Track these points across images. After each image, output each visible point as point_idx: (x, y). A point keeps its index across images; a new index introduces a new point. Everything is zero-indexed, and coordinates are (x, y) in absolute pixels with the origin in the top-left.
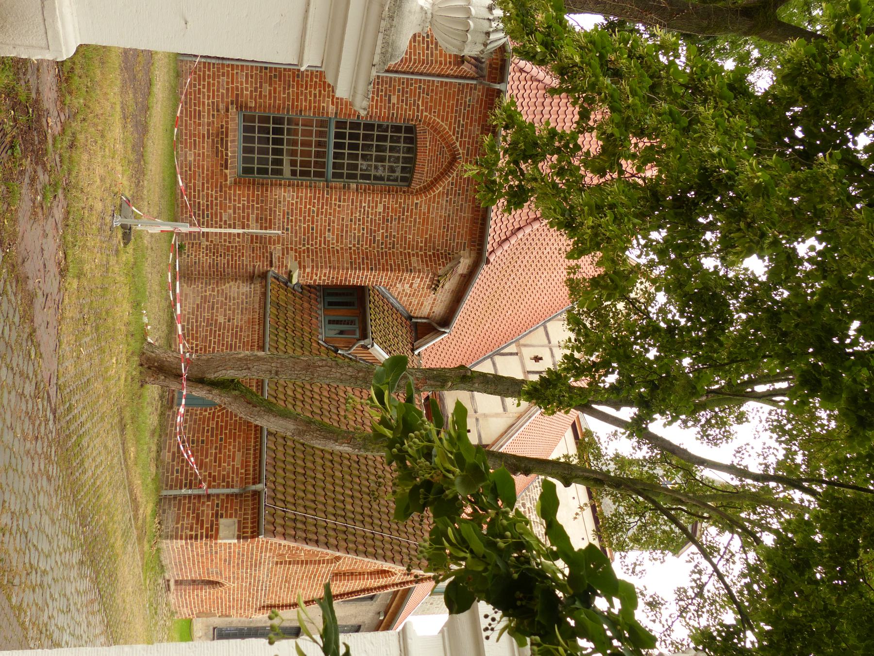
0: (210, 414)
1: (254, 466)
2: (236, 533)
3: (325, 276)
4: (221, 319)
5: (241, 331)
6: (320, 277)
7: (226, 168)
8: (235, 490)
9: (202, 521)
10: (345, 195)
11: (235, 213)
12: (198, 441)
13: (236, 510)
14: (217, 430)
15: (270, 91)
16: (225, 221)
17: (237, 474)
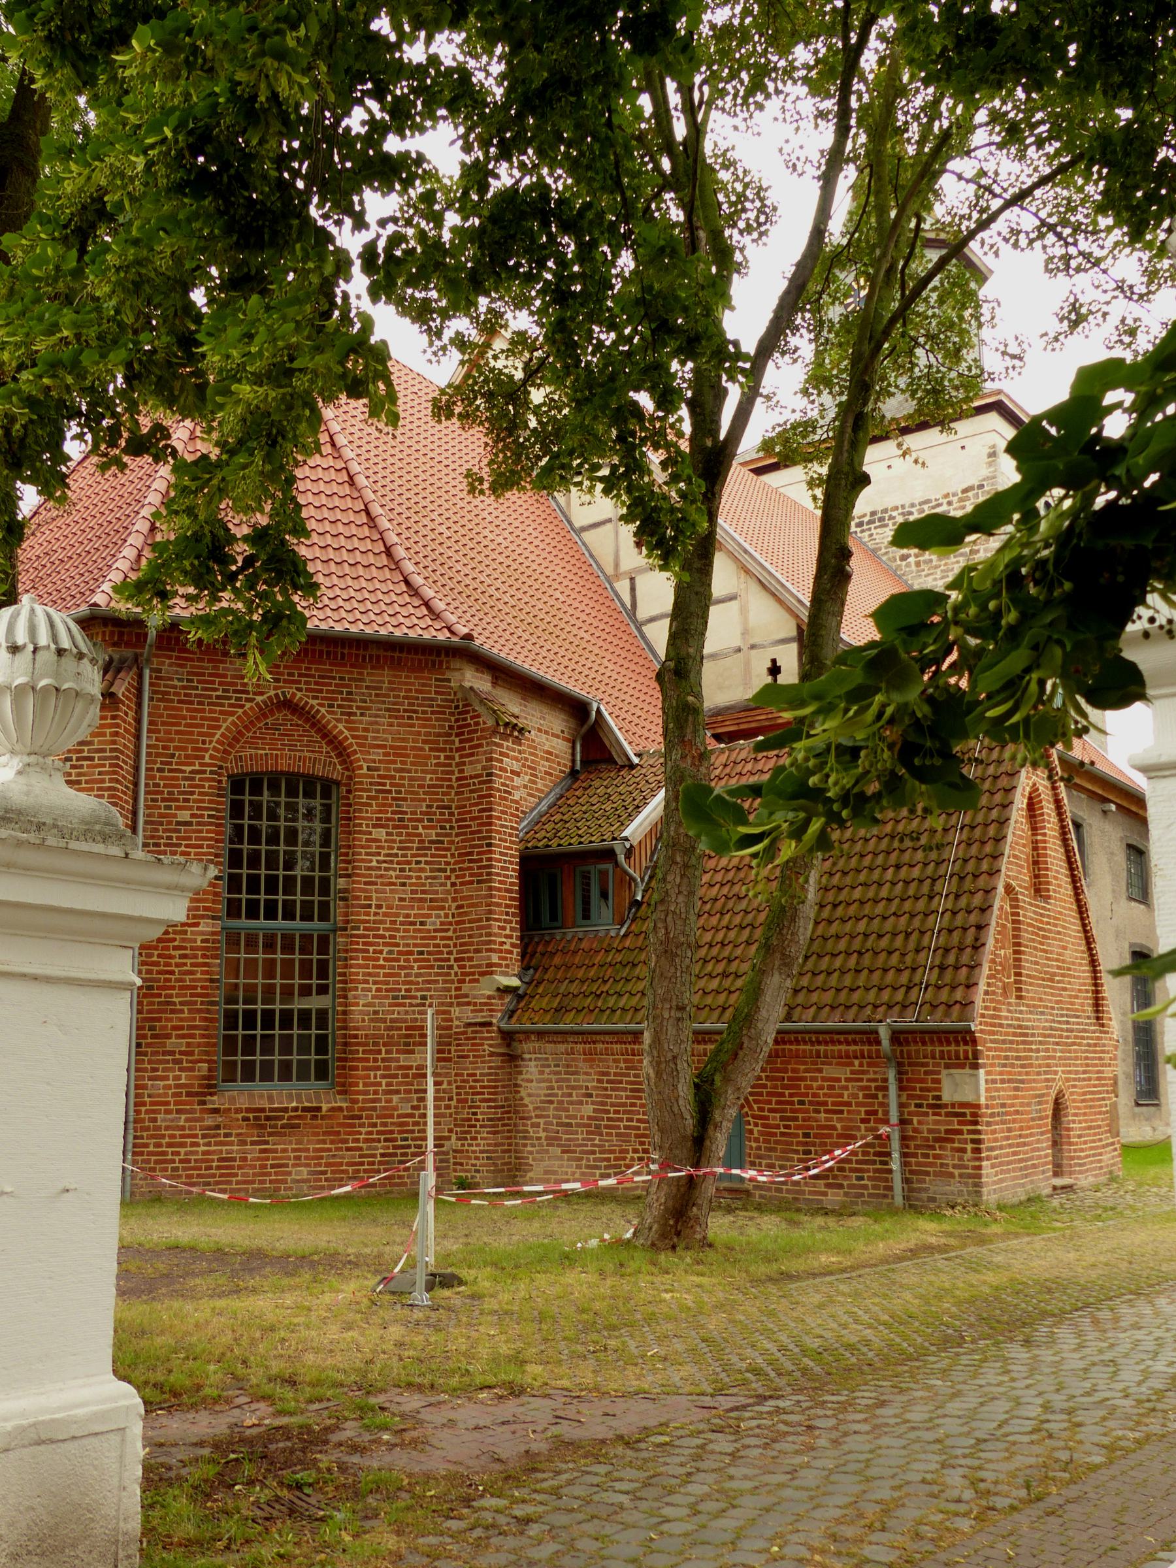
0: (756, 1125)
1: (848, 1044)
2: (967, 1070)
4: (588, 1110)
5: (607, 1074)
6: (506, 936)
7: (319, 1109)
8: (892, 1075)
9: (947, 1131)
11: (398, 1092)
12: (806, 1144)
14: (785, 1111)
16: (413, 1108)
17: (863, 1072)
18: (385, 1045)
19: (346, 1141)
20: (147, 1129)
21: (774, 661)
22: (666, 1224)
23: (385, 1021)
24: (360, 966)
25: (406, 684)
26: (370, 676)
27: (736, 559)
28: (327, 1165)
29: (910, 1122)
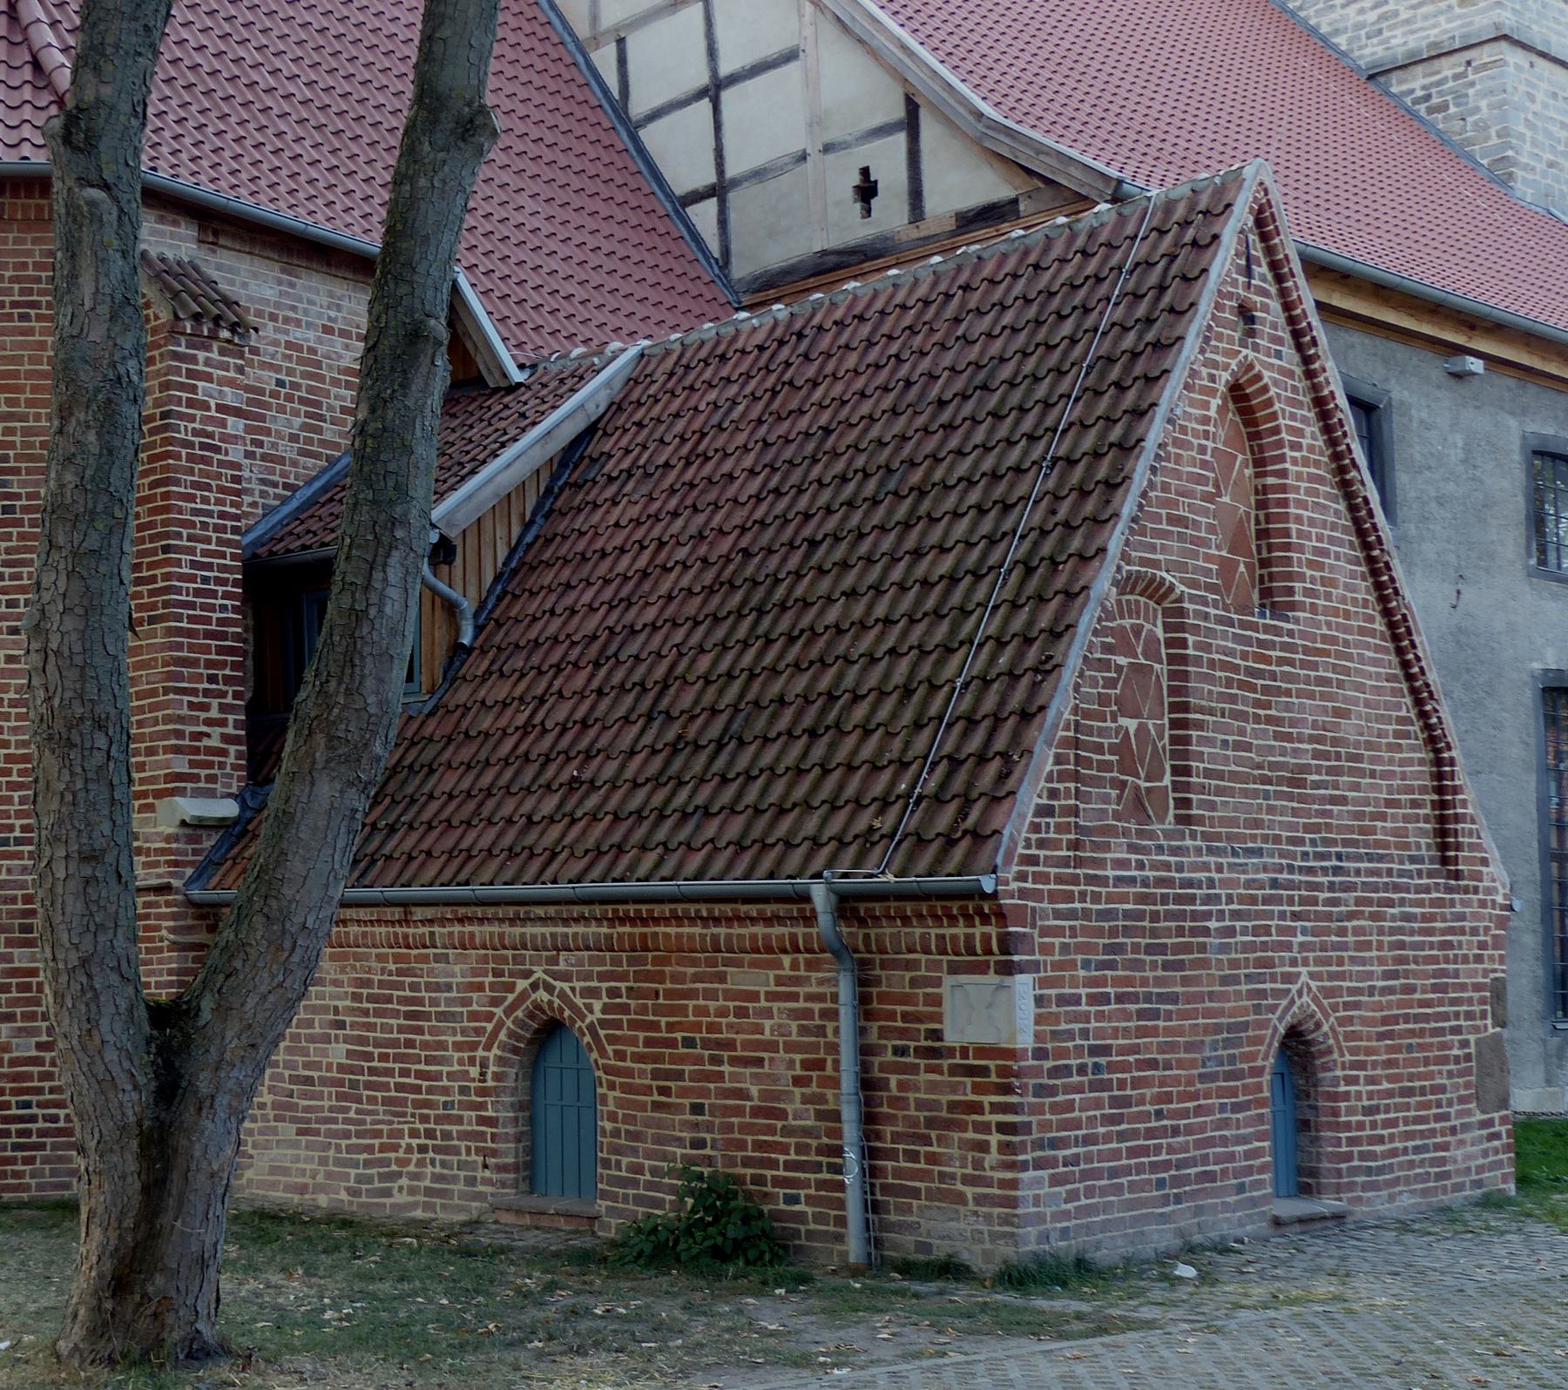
0: (612, 1086)
1: (768, 921)
2: (992, 978)
3: (205, 707)
4: (338, 1052)
5: (367, 983)
6: (209, 722)
8: (846, 989)
9: (953, 1106)
12: (696, 1126)
13: (914, 982)
16: (39, 1046)
17: (797, 981)
21: (865, 172)
22: (99, 1308)
25: (15, 253)
29: (884, 1085)
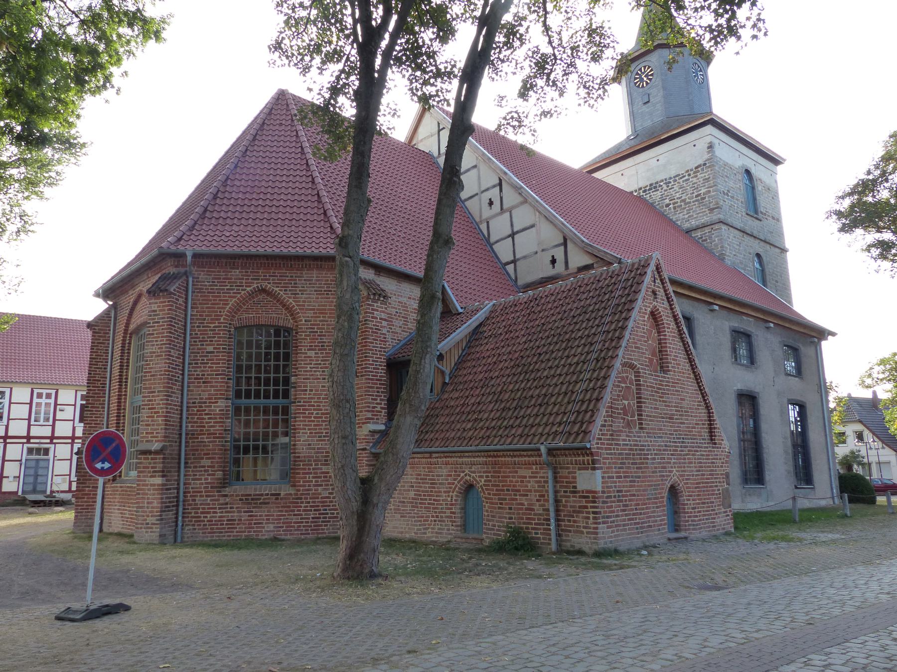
2: (590, 471)
4: (412, 494)
5: (420, 475)
7: (279, 494)
8: (550, 474)
9: (580, 507)
10: (300, 386)
11: (321, 485)
12: (510, 513)
13: (569, 473)
14: (500, 495)
15: (207, 458)
17: (537, 473)
18: (315, 461)
19: (294, 511)
20: (191, 505)
21: (553, 256)
23: (314, 449)
24: (301, 421)
26: (305, 274)
27: (534, 207)
28: (283, 523)
29: (561, 501)
